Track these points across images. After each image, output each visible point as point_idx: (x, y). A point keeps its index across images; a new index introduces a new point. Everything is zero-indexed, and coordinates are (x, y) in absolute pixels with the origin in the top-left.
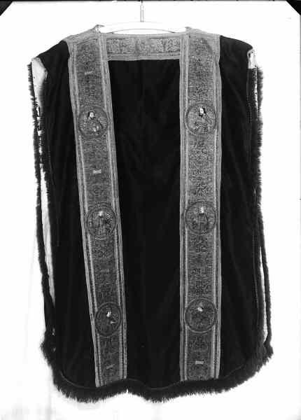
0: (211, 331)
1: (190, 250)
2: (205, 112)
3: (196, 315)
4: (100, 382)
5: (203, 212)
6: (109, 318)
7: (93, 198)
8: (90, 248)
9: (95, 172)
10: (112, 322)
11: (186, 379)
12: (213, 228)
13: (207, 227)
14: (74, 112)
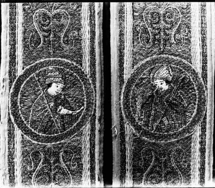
0: (189, 138)
3: (153, 98)
6: (57, 98)
10: (64, 111)
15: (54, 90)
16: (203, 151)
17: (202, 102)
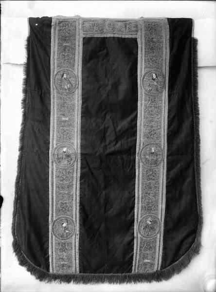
1: (143, 179)
2: (156, 77)
3: (147, 226)
4: (53, 270)
5: (153, 151)
7: (60, 138)
8: (54, 173)
9: (64, 119)
11: (136, 271)
12: (160, 163)
13: (156, 163)
14: (52, 71)
15: (64, 225)
16: (160, 241)
17: (160, 227)
